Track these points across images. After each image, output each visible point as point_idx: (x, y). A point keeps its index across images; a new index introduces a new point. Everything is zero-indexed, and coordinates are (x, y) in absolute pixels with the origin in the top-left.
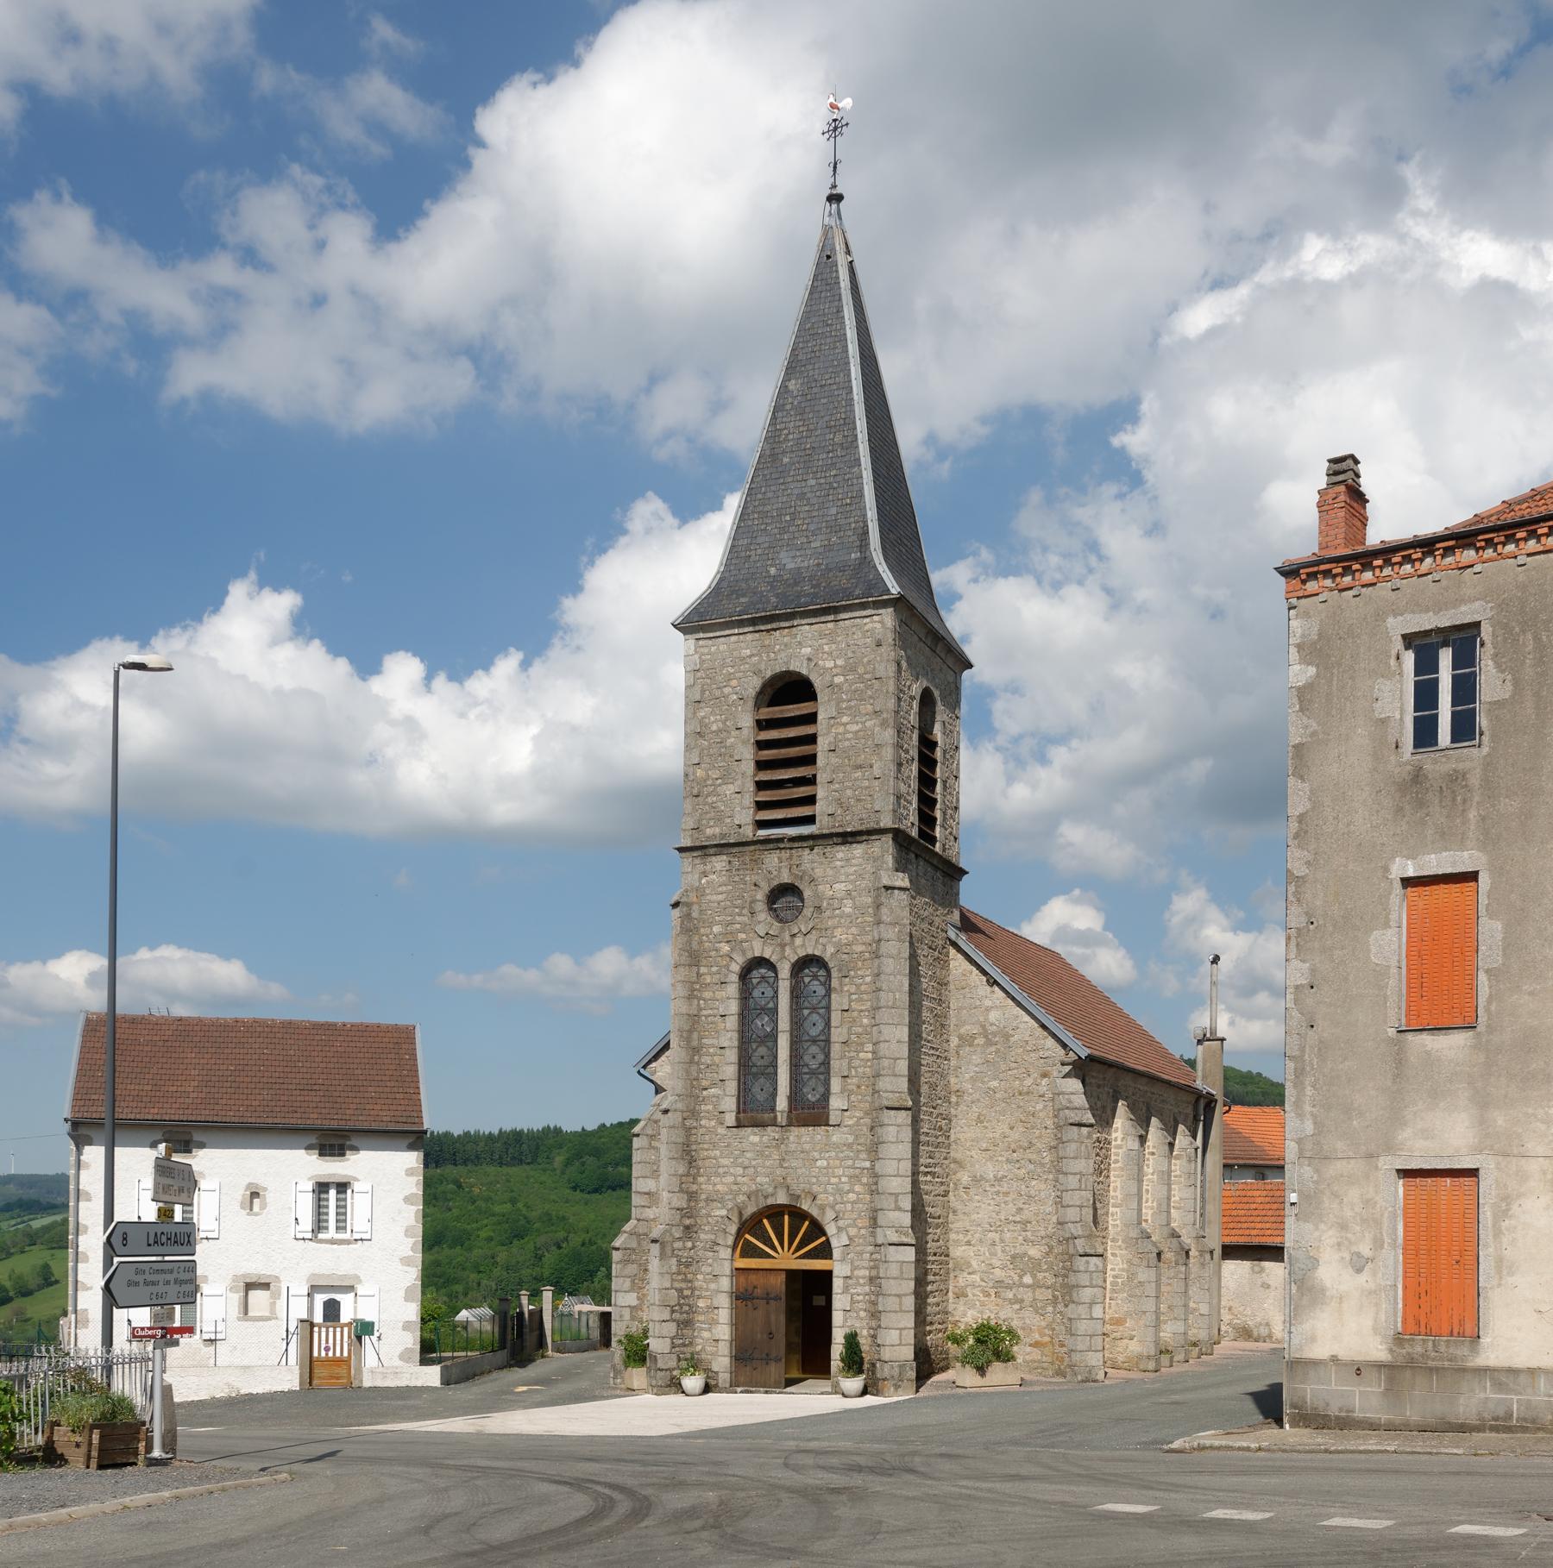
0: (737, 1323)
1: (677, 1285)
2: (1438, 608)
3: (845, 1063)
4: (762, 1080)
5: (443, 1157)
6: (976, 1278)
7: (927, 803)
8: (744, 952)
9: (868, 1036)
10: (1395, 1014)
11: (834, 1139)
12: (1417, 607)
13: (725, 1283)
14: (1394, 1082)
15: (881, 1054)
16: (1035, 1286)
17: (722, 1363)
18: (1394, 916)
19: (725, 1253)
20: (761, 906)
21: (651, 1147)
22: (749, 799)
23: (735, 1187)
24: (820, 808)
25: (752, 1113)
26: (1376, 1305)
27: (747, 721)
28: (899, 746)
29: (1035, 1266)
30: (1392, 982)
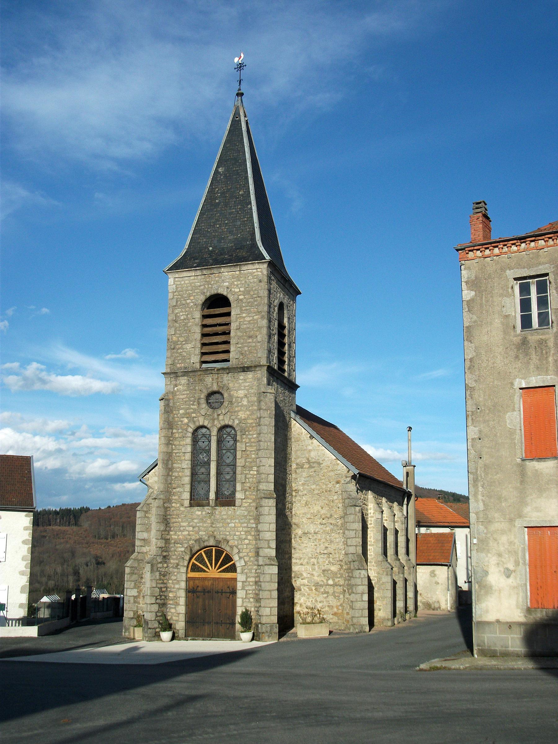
0: (189, 604)
1: (159, 586)
2: (529, 267)
3: (243, 476)
4: (202, 484)
5: (41, 520)
6: (305, 581)
7: (281, 354)
8: (194, 422)
9: (255, 464)
10: (520, 452)
11: (238, 513)
12: (519, 266)
13: (183, 585)
14: (521, 484)
15: (261, 472)
16: (335, 585)
17: (180, 625)
18: (517, 406)
19: (183, 570)
20: (203, 401)
21: (145, 517)
22: (198, 351)
23: (189, 537)
24: (232, 355)
25: (197, 500)
26: (518, 594)
27: (198, 315)
28: (269, 327)
29: (334, 575)
30: (517, 437)
